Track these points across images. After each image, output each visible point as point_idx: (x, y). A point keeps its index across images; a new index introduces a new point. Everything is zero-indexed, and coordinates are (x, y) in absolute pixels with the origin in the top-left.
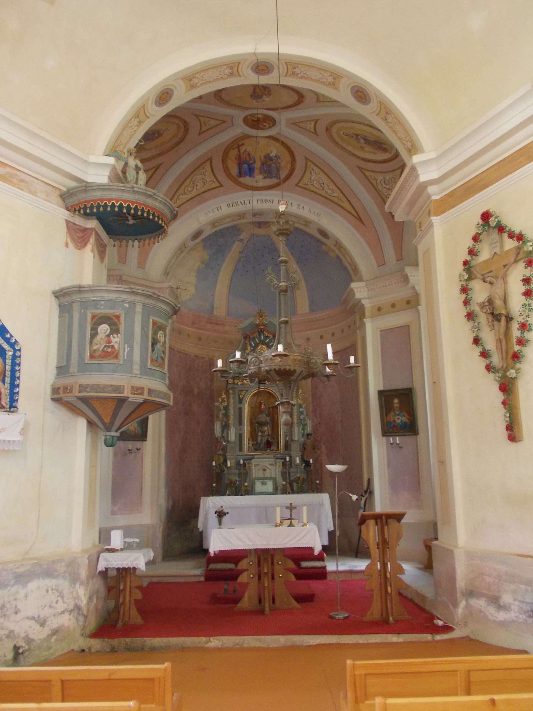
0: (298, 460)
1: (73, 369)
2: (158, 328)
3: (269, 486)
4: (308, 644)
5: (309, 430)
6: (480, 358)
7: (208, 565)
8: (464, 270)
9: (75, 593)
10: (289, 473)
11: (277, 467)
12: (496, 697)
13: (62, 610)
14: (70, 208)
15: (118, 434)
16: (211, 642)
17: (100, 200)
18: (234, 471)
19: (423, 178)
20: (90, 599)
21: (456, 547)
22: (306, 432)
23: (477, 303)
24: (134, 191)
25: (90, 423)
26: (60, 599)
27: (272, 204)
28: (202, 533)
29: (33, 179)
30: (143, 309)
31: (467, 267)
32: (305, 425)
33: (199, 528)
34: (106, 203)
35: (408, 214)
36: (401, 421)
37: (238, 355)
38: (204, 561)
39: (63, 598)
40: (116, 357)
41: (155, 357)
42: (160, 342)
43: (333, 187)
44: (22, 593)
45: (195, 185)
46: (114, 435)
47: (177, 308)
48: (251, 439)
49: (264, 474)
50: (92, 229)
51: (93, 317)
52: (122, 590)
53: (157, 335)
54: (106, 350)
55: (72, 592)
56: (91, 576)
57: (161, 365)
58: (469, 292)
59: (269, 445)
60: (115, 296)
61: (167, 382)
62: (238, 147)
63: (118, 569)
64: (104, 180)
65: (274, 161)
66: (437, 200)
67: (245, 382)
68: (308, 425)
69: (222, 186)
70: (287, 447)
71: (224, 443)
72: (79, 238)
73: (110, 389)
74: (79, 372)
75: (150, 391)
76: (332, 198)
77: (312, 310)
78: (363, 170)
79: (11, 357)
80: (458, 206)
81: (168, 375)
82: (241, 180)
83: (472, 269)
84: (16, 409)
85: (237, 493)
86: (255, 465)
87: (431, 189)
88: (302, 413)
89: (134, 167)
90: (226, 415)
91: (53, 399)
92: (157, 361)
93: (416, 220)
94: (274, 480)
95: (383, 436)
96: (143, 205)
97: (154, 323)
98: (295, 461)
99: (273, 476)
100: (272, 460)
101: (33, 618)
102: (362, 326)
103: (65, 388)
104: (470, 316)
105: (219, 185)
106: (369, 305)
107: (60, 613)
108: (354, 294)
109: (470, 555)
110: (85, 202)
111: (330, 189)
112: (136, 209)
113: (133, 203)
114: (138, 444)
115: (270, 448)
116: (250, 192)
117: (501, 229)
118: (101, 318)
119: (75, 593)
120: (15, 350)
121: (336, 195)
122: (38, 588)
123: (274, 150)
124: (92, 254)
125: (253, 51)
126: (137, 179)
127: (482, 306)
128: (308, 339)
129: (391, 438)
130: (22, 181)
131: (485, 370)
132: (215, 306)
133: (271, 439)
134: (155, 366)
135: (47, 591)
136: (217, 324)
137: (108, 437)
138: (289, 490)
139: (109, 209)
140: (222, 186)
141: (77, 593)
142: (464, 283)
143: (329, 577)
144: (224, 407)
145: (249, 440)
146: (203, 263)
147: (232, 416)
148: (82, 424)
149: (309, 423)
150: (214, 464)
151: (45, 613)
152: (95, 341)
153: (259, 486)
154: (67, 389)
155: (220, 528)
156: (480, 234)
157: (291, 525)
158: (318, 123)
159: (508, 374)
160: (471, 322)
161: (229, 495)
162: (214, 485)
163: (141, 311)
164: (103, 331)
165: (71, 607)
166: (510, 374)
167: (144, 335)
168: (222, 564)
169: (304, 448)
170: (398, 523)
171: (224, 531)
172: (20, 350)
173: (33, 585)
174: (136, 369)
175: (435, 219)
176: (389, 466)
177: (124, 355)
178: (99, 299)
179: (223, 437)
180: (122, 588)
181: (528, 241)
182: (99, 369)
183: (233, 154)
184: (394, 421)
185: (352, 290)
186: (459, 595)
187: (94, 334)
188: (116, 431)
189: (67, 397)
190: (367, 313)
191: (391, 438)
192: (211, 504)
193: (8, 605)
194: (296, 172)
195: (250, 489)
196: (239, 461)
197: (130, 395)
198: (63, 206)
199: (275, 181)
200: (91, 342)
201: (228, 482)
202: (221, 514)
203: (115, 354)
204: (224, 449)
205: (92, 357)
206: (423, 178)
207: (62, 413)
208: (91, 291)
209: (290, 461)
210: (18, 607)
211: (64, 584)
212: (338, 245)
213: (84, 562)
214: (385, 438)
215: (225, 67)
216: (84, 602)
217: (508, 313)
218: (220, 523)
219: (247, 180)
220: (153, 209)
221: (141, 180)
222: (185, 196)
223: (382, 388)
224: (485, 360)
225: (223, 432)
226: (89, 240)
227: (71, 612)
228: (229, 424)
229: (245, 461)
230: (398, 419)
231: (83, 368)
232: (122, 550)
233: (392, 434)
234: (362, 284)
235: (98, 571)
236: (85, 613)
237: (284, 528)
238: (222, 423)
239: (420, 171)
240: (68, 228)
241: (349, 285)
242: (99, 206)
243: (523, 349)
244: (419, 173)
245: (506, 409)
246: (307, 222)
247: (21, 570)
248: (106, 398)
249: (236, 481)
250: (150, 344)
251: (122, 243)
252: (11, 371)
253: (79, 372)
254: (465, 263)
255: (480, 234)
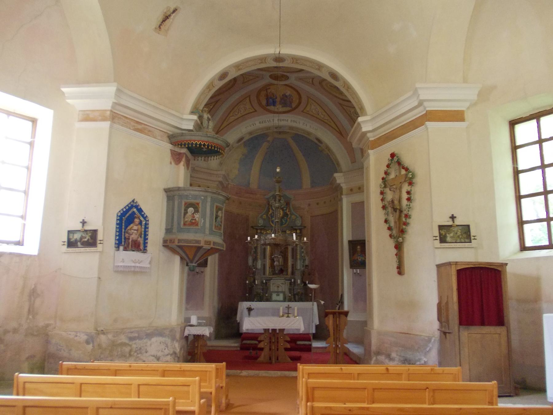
0: (299, 281)
1: (175, 230)
2: (219, 209)
3: (281, 297)
4: (292, 376)
5: (307, 263)
6: (387, 230)
7: (242, 342)
8: (382, 182)
9: (173, 346)
10: (294, 289)
11: (286, 285)
12: (342, 368)
13: (167, 353)
14: (173, 143)
15: (196, 265)
16: (243, 373)
17: (189, 140)
18: (259, 287)
19: (364, 129)
20: (181, 349)
21: (373, 329)
22: (305, 265)
23: (387, 201)
24: (207, 136)
25: (182, 258)
26: (166, 348)
27: (287, 122)
28: (239, 323)
29: (154, 129)
30: (211, 200)
31: (384, 180)
32: (304, 260)
33: (237, 321)
34: (192, 142)
35: (359, 144)
36: (361, 259)
37: (256, 237)
38: (240, 340)
39: (167, 347)
40: (197, 225)
41: (217, 225)
42: (219, 216)
43: (324, 114)
44: (149, 343)
45: (240, 111)
46: (194, 265)
47: (229, 198)
48: (271, 268)
49: (278, 289)
50: (184, 153)
51: (186, 204)
52: (196, 347)
53: (218, 213)
54: (192, 221)
55: (172, 345)
56: (181, 338)
57: (220, 229)
58: (384, 195)
59: (281, 271)
60: (197, 193)
61: (223, 238)
62: (267, 90)
63: (194, 335)
64: (191, 127)
65: (288, 98)
66: (372, 141)
67: (268, 232)
68: (307, 260)
69: (256, 111)
70: (293, 273)
71: (254, 270)
72: (177, 158)
73: (194, 242)
74: (178, 232)
75: (214, 243)
76: (325, 121)
77: (312, 187)
78: (343, 106)
79: (144, 224)
80: (382, 146)
81: (223, 234)
82: (268, 107)
83: (386, 182)
84: (146, 251)
85: (261, 300)
86: (273, 283)
87: (369, 135)
88: (303, 252)
89: (207, 119)
90: (256, 252)
91: (163, 246)
92: (217, 227)
93: (364, 148)
94: (284, 293)
95: (351, 268)
96: (212, 143)
97: (217, 207)
98: (297, 282)
99: (284, 290)
100: (283, 281)
101: (154, 356)
102: (341, 200)
103: (171, 241)
104: (384, 207)
105: (254, 111)
106: (346, 187)
107: (166, 354)
108: (336, 180)
109: (379, 333)
110: (182, 141)
111: (323, 115)
112: (208, 145)
113: (207, 142)
114: (202, 269)
115: (283, 273)
116: (272, 115)
117: (399, 163)
118: (189, 204)
119: (173, 346)
120: (146, 221)
121: (326, 118)
122: (156, 341)
123: (288, 92)
124: (183, 167)
125: (274, 53)
126: (208, 126)
127: (389, 202)
128: (309, 205)
129: (355, 270)
130: (150, 131)
131: (389, 237)
132: (251, 182)
133: (283, 268)
134: (217, 230)
135: (160, 343)
136: (252, 194)
137: (191, 266)
138: (293, 300)
139: (194, 146)
140: (256, 111)
141: (175, 346)
142: (382, 190)
143: (313, 351)
144: (254, 247)
145: (269, 268)
146: (243, 155)
147: (259, 253)
148: (177, 259)
149: (307, 258)
150: (247, 282)
151: (159, 354)
152: (186, 216)
153: (274, 297)
154: (172, 241)
155: (249, 317)
156: (390, 164)
157: (288, 317)
158: (314, 79)
159: (398, 240)
160: (385, 210)
161: (256, 302)
162: (247, 295)
163: (210, 200)
164: (190, 211)
165: (171, 352)
166: (400, 240)
167: (212, 214)
168: (251, 341)
169: (303, 274)
170: (345, 317)
171: (251, 319)
172: (148, 221)
173: (154, 339)
174: (207, 232)
175: (370, 152)
176: (353, 286)
177: (201, 224)
178: (188, 194)
179: (253, 266)
180: (196, 345)
181: (410, 172)
182: (189, 231)
183: (263, 93)
184: (357, 259)
185: (335, 178)
186: (372, 354)
187: (186, 213)
188: (195, 263)
189: (171, 245)
190: (344, 192)
191: (355, 270)
192: (245, 306)
193: (142, 348)
194: (302, 104)
195: (269, 298)
196: (263, 281)
197: (204, 245)
198: (169, 142)
199: (288, 109)
200: (184, 217)
201: (255, 293)
202: (250, 310)
203: (196, 224)
204: (254, 273)
205: (184, 224)
206: (364, 129)
207: (168, 253)
208: (185, 190)
209: (294, 281)
210: (147, 350)
211: (168, 341)
212: (327, 147)
213: (178, 330)
214: (351, 269)
215: (258, 60)
216: (178, 350)
217: (400, 208)
218: (249, 314)
219: (272, 108)
220: (217, 144)
221: (210, 126)
222: (233, 117)
223: (351, 239)
224: (390, 231)
225: (253, 262)
226: (182, 159)
227: (171, 355)
228: (257, 258)
229: (267, 281)
230: (360, 258)
231: (180, 230)
232: (196, 326)
233: (359, 267)
234: (341, 174)
235: (184, 336)
236: (178, 356)
237: (284, 318)
238: (253, 257)
239: (362, 125)
240: (171, 154)
241: (332, 174)
242: (189, 144)
243: (407, 227)
244: (362, 126)
245: (397, 258)
246: (309, 133)
247: (148, 332)
248: (192, 246)
249: (261, 293)
250: (214, 218)
251: (199, 158)
252: (144, 231)
253: (178, 232)
254: (383, 179)
255: (390, 164)
